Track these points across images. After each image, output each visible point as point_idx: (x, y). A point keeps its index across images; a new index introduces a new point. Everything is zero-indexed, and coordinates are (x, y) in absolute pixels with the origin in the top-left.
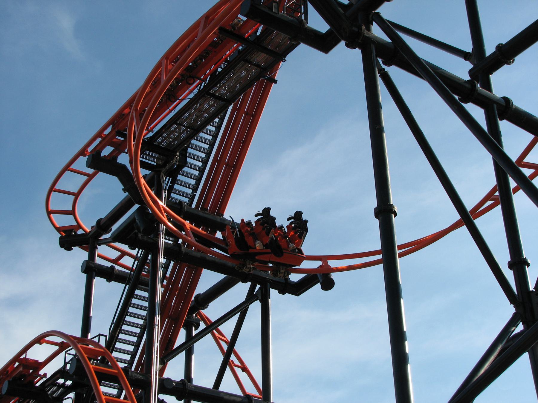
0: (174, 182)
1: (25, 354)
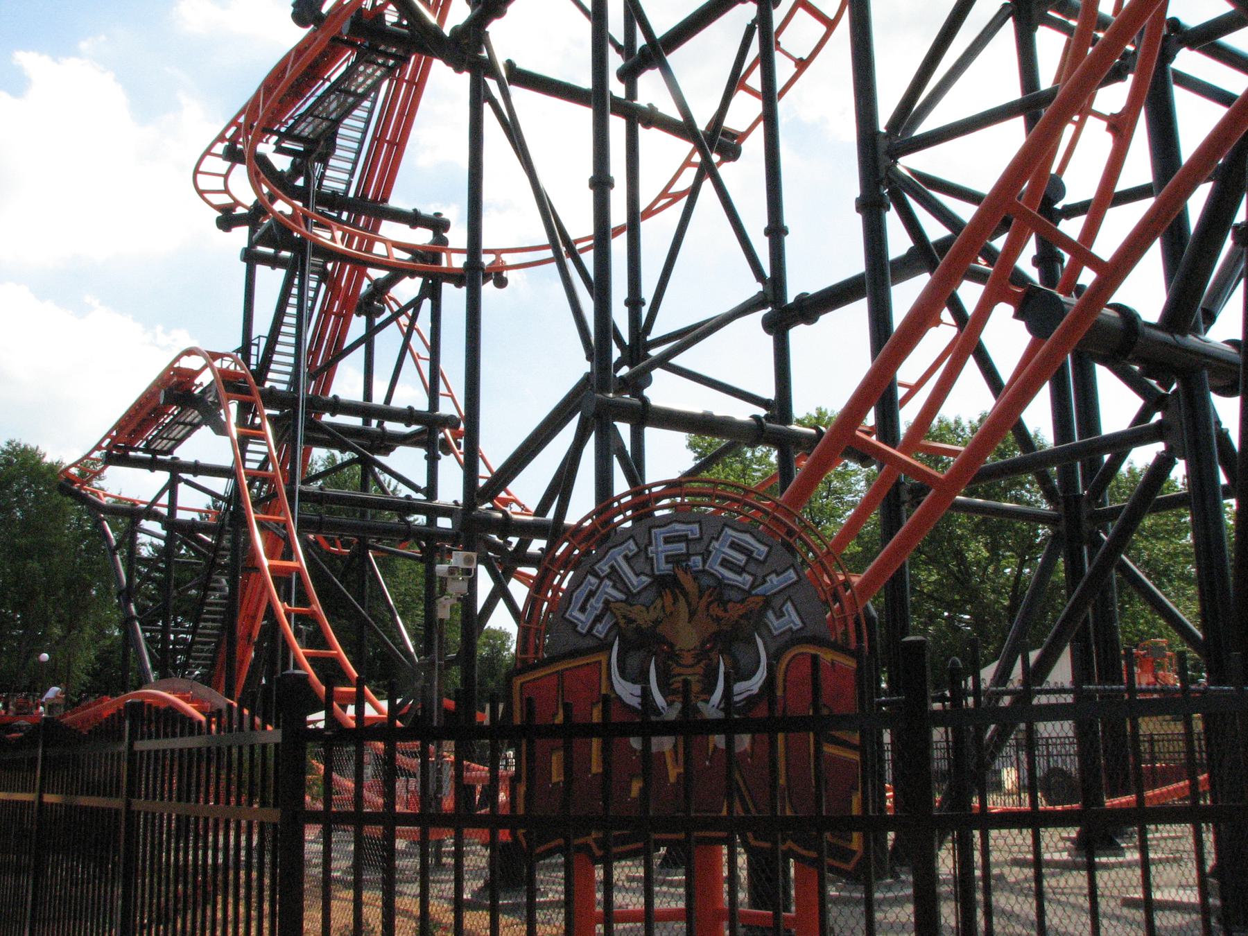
0: (326, 166)
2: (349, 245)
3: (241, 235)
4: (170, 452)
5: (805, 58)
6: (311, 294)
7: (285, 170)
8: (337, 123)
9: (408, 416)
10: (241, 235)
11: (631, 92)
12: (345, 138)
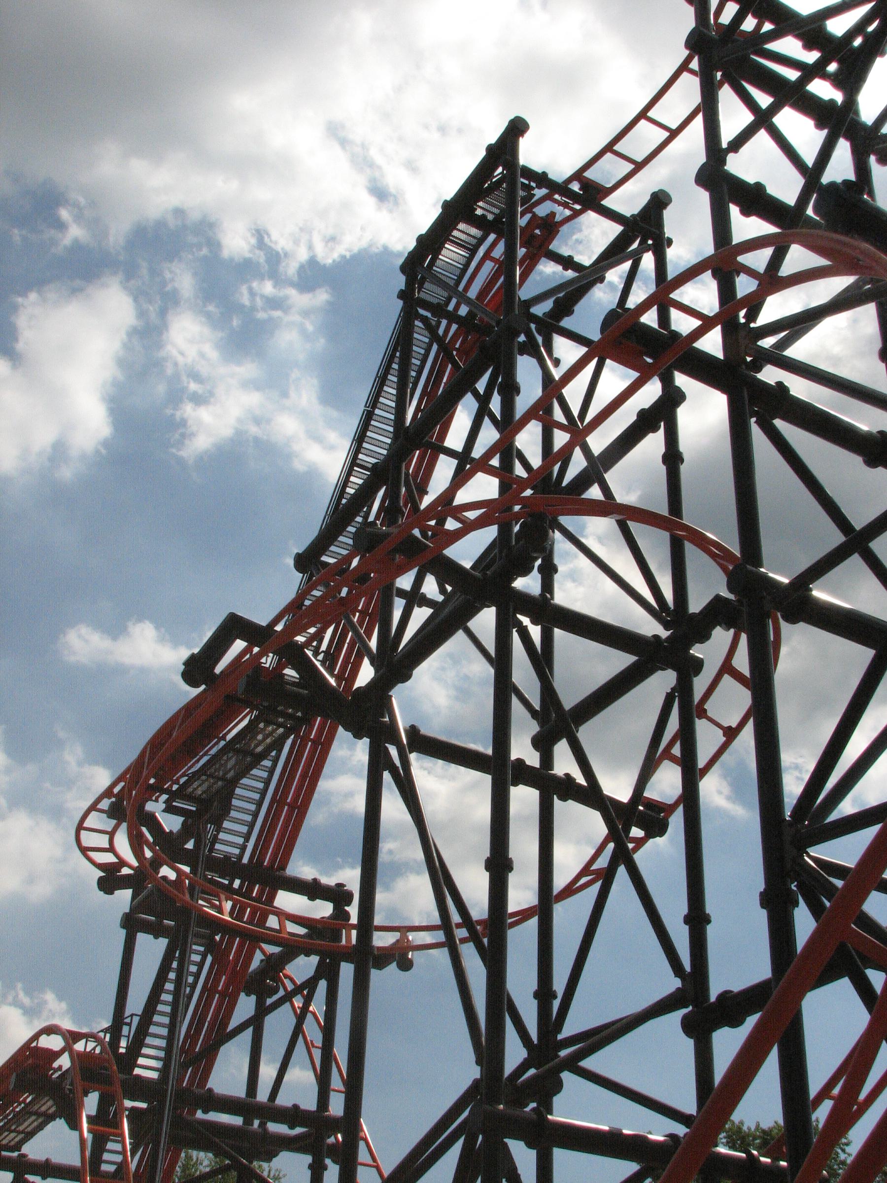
0: (219, 829)
1: (36, 1042)
2: (239, 918)
3: (125, 896)
4: (18, 1147)
5: (734, 725)
6: (191, 979)
7: (175, 831)
8: (233, 783)
9: (293, 1115)
10: (125, 896)
11: (547, 760)
12: (242, 798)
